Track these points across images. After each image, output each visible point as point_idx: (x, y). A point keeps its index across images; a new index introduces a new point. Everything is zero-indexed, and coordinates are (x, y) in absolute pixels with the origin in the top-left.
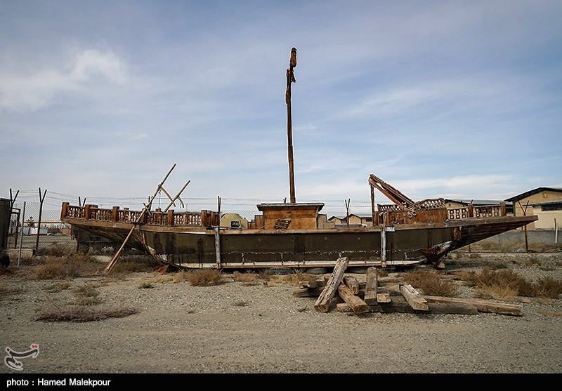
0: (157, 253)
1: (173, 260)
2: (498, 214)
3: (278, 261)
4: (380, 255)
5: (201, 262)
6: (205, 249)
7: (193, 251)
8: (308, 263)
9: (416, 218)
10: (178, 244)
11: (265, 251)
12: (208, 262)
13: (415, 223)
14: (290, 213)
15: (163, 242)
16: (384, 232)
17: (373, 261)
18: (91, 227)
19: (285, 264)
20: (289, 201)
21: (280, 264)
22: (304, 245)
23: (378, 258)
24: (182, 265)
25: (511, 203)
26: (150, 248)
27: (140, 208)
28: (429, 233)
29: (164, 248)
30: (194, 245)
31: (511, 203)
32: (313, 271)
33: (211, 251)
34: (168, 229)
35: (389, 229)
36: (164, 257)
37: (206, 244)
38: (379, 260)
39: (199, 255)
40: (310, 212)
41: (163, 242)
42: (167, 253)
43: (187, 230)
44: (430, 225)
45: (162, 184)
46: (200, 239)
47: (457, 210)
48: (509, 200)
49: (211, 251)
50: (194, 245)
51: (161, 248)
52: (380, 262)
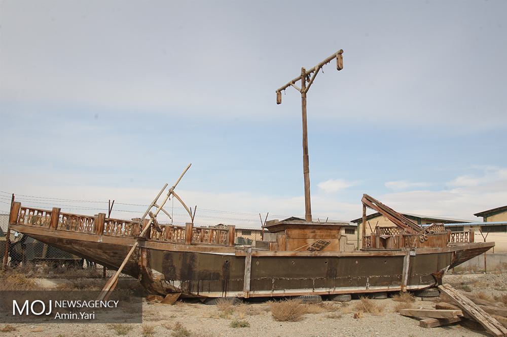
0: (167, 279)
1: (190, 288)
2: (454, 240)
3: (309, 287)
4: (401, 279)
5: (225, 289)
6: (232, 274)
7: (216, 276)
8: (339, 290)
9: (426, 242)
10: (198, 268)
11: (298, 276)
12: (233, 290)
13: (426, 247)
14: (314, 232)
15: (178, 264)
16: (408, 256)
17: (395, 286)
18: (60, 240)
19: (317, 291)
20: (302, 215)
21: (310, 291)
22: (336, 270)
23: (399, 283)
24: (201, 294)
25: (356, 224)
26: (154, 272)
27: (210, 292)
28: (439, 258)
29: (178, 272)
30: (219, 269)
31: (356, 224)
32: (342, 298)
33: (238, 277)
34: (187, 248)
35: (412, 253)
36: (177, 284)
37: (233, 268)
38: (399, 285)
39: (223, 282)
40: (334, 232)
41: (178, 264)
42: (183, 278)
43: (212, 249)
44: (440, 250)
45: (156, 200)
46: (227, 262)
47: (457, 233)
48: (354, 221)
49: (238, 277)
50: (219, 269)
51: (174, 272)
52: (400, 287)
